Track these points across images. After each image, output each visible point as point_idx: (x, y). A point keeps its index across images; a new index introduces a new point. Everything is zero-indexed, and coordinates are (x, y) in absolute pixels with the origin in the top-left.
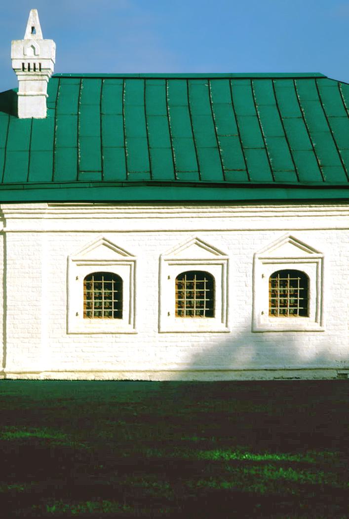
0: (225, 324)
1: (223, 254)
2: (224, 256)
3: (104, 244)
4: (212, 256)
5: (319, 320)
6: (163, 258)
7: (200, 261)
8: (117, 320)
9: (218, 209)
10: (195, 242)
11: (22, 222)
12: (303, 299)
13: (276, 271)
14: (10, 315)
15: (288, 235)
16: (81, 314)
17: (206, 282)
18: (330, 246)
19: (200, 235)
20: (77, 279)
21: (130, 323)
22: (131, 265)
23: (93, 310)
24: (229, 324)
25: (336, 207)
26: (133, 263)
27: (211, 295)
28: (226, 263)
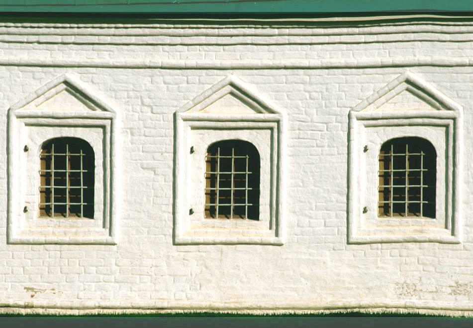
0: (274, 231)
1: (272, 112)
2: (105, 112)
3: (232, 93)
4: (426, 109)
5: (108, 225)
6: (181, 115)
7: (409, 120)
8: (87, 220)
9: (369, 28)
10: (229, 91)
11: (365, 50)
12: (86, 187)
13: (86, 139)
14: (4, 211)
15: (402, 79)
16: (35, 210)
17: (83, 156)
18: (453, 90)
19: (237, 77)
20: (192, 151)
21: (270, 228)
22: (447, 126)
23: (68, 204)
24: (281, 231)
25: (253, 29)
26: (451, 122)
27: (255, 181)
28: (276, 126)
